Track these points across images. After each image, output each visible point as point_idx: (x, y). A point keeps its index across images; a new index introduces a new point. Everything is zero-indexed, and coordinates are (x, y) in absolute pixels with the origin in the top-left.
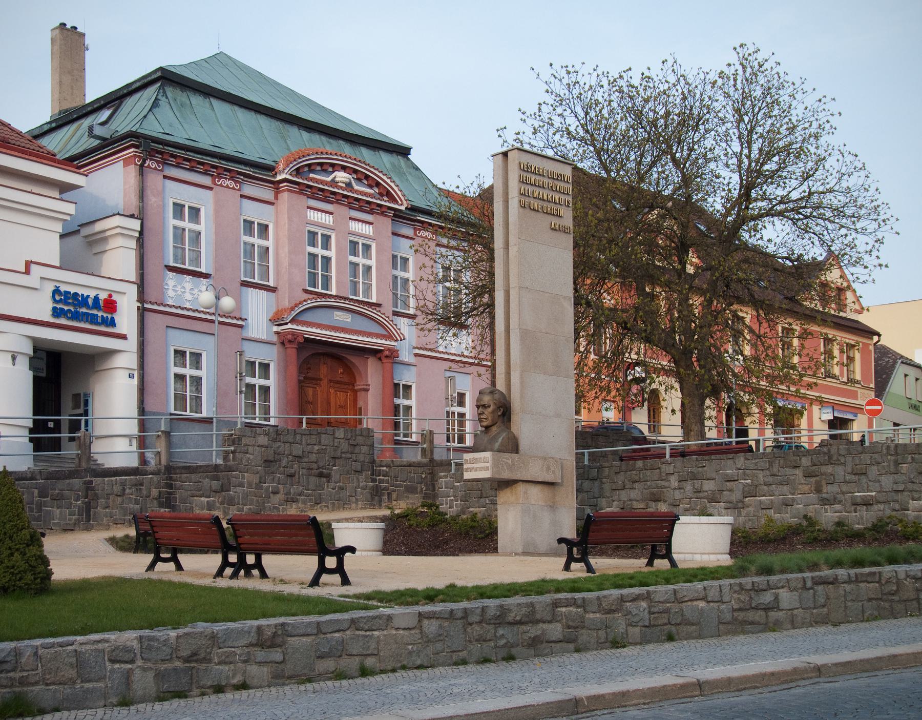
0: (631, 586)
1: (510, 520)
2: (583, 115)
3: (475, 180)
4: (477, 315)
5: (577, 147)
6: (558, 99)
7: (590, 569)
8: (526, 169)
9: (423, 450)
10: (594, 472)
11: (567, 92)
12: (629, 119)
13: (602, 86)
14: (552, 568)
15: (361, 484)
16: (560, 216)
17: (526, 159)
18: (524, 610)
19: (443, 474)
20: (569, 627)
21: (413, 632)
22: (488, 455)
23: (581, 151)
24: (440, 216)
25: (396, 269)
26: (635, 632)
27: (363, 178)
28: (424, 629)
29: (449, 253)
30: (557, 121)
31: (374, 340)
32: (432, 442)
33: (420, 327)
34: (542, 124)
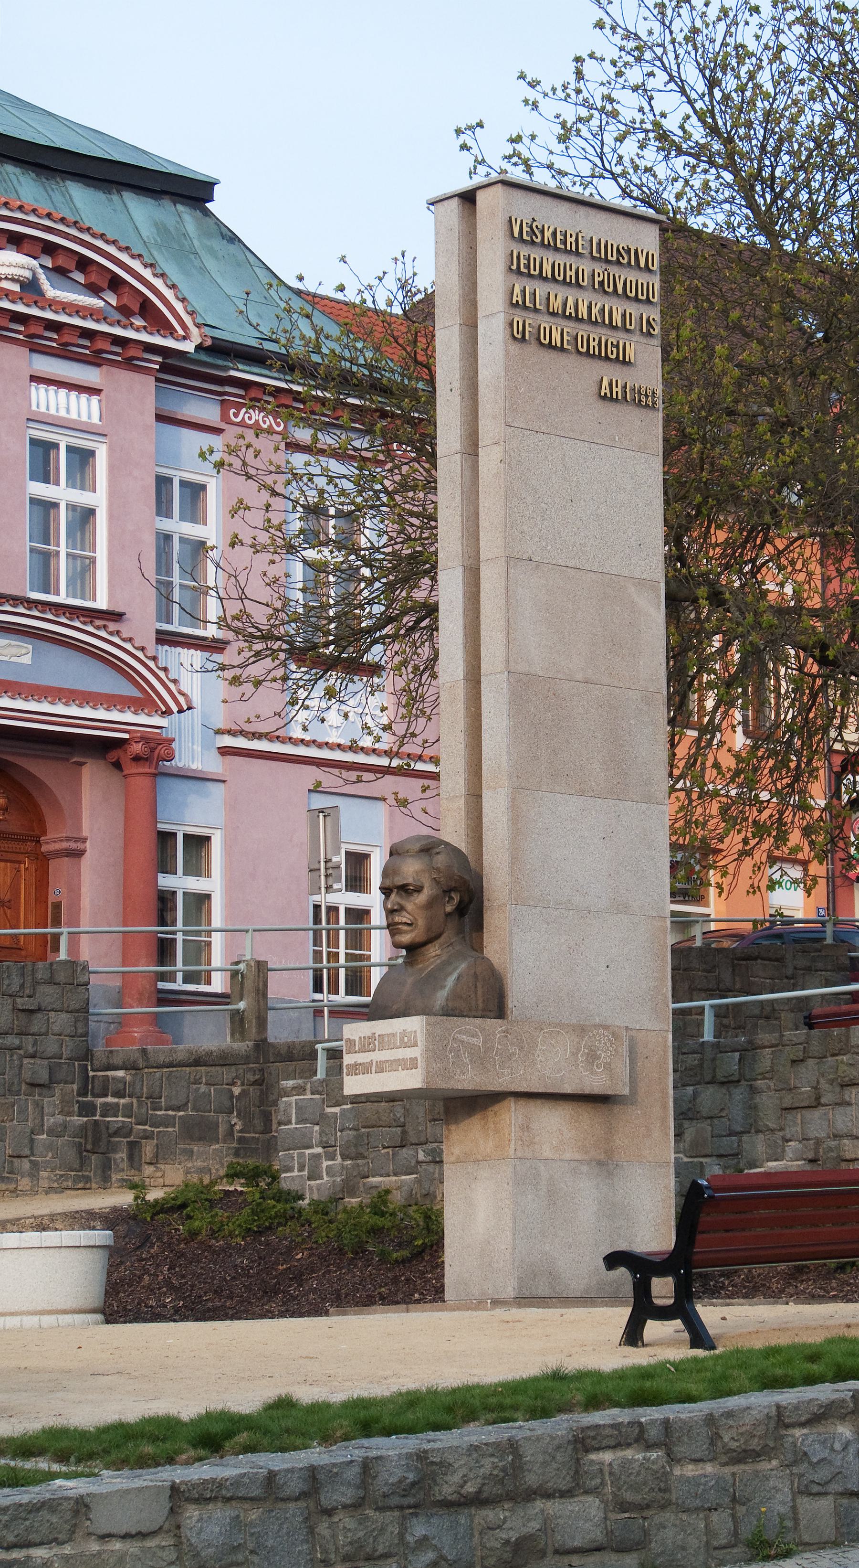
0: (810, 1380)
1: (482, 1207)
2: (701, 86)
3: (390, 267)
4: (394, 637)
5: (685, 173)
6: (631, 44)
7: (698, 1336)
8: (528, 236)
9: (238, 1019)
10: (731, 1063)
11: (657, 27)
12: (833, 95)
13: (756, 10)
14: (591, 1339)
15: (49, 1121)
16: (625, 363)
17: (526, 209)
18: (487, 1462)
19: (290, 1083)
20: (623, 1506)
21: (151, 1543)
22: (414, 1024)
23: (697, 183)
24: (289, 366)
25: (169, 515)
26: (821, 1511)
27: (68, 265)
28: (185, 1532)
29: (317, 470)
30: (629, 105)
31: (101, 714)
32: (261, 992)
33: (229, 674)
34: (584, 112)
